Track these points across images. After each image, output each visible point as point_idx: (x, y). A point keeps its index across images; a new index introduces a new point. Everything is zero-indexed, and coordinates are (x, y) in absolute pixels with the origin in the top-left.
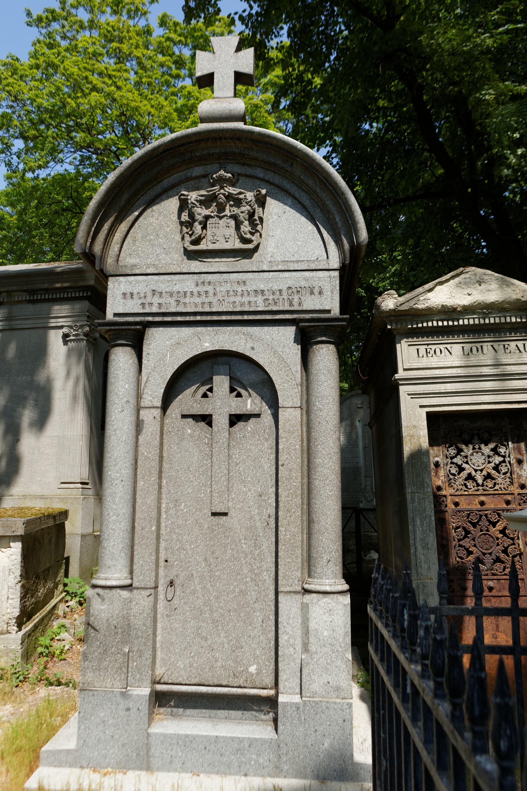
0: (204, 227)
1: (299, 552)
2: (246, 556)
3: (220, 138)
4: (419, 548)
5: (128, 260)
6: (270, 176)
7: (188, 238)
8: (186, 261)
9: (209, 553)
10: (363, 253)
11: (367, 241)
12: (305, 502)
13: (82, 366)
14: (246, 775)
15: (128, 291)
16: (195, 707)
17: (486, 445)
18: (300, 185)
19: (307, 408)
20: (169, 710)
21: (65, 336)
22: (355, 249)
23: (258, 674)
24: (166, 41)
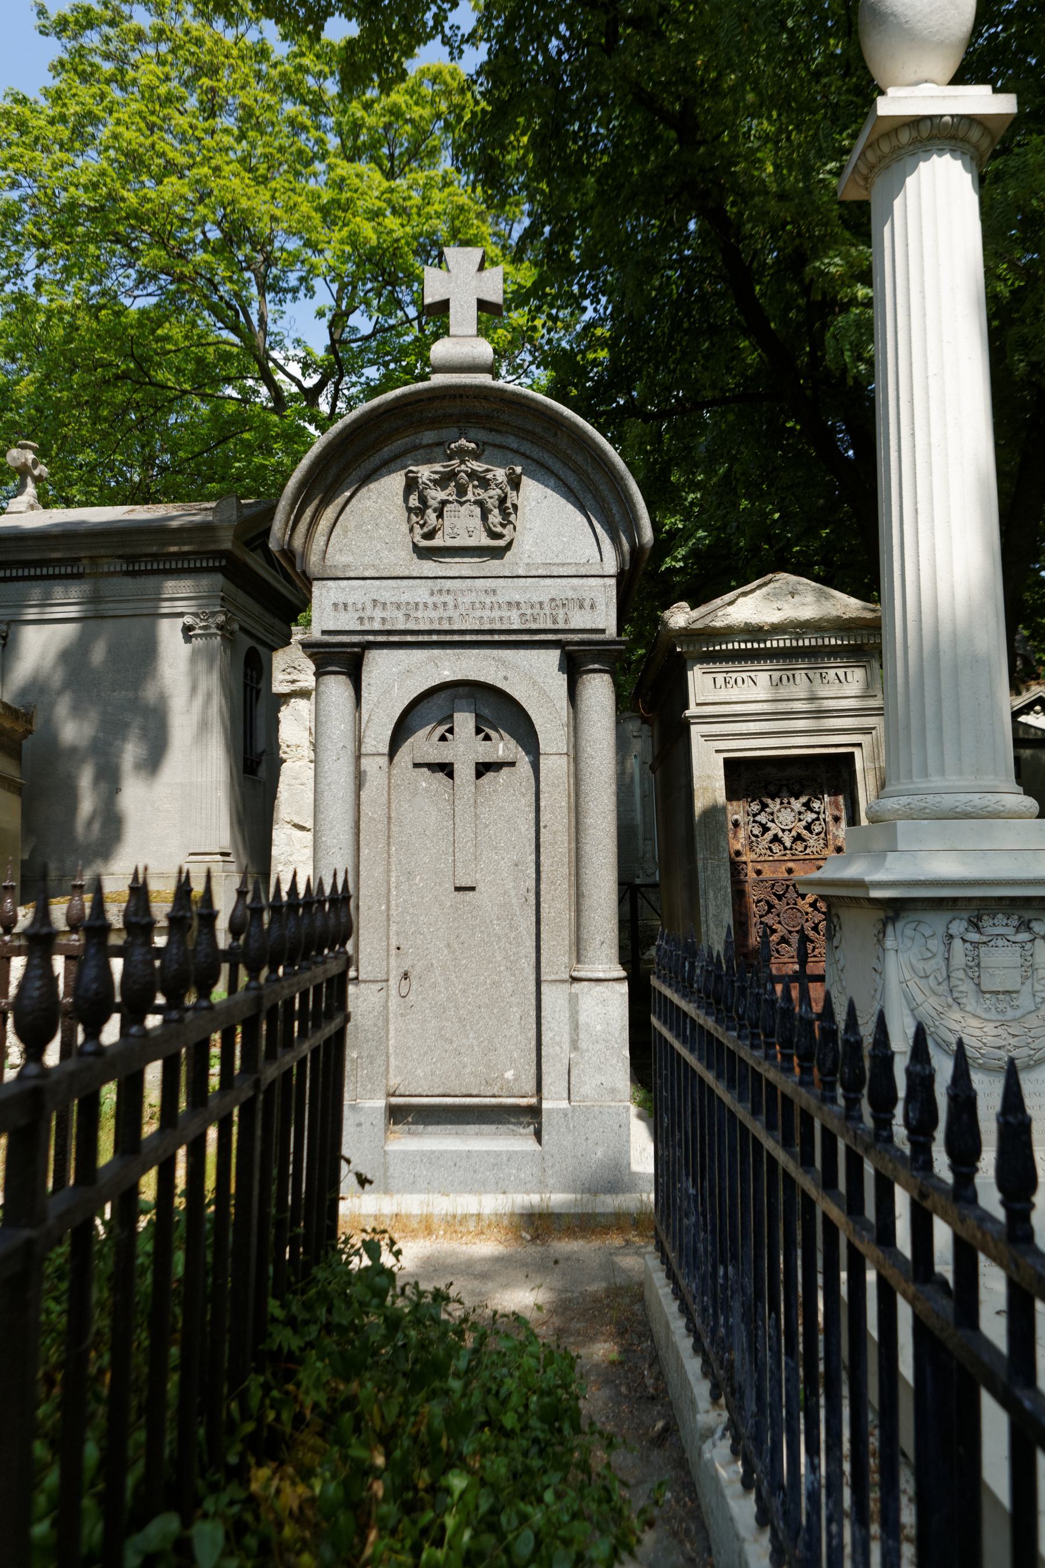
0: (440, 516)
1: (565, 933)
2: (499, 939)
3: (461, 396)
4: (712, 925)
5: (339, 557)
6: (526, 447)
7: (418, 530)
8: (416, 560)
9: (453, 937)
10: (647, 556)
11: (652, 543)
12: (573, 872)
13: (215, 676)
14: (504, 1193)
15: (341, 601)
16: (438, 1123)
17: (797, 798)
18: (566, 461)
19: (575, 754)
20: (406, 1127)
21: (187, 629)
22: (637, 551)
23: (515, 1080)
24: (295, 72)
